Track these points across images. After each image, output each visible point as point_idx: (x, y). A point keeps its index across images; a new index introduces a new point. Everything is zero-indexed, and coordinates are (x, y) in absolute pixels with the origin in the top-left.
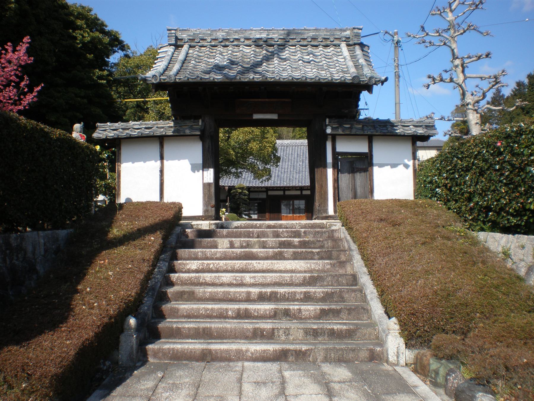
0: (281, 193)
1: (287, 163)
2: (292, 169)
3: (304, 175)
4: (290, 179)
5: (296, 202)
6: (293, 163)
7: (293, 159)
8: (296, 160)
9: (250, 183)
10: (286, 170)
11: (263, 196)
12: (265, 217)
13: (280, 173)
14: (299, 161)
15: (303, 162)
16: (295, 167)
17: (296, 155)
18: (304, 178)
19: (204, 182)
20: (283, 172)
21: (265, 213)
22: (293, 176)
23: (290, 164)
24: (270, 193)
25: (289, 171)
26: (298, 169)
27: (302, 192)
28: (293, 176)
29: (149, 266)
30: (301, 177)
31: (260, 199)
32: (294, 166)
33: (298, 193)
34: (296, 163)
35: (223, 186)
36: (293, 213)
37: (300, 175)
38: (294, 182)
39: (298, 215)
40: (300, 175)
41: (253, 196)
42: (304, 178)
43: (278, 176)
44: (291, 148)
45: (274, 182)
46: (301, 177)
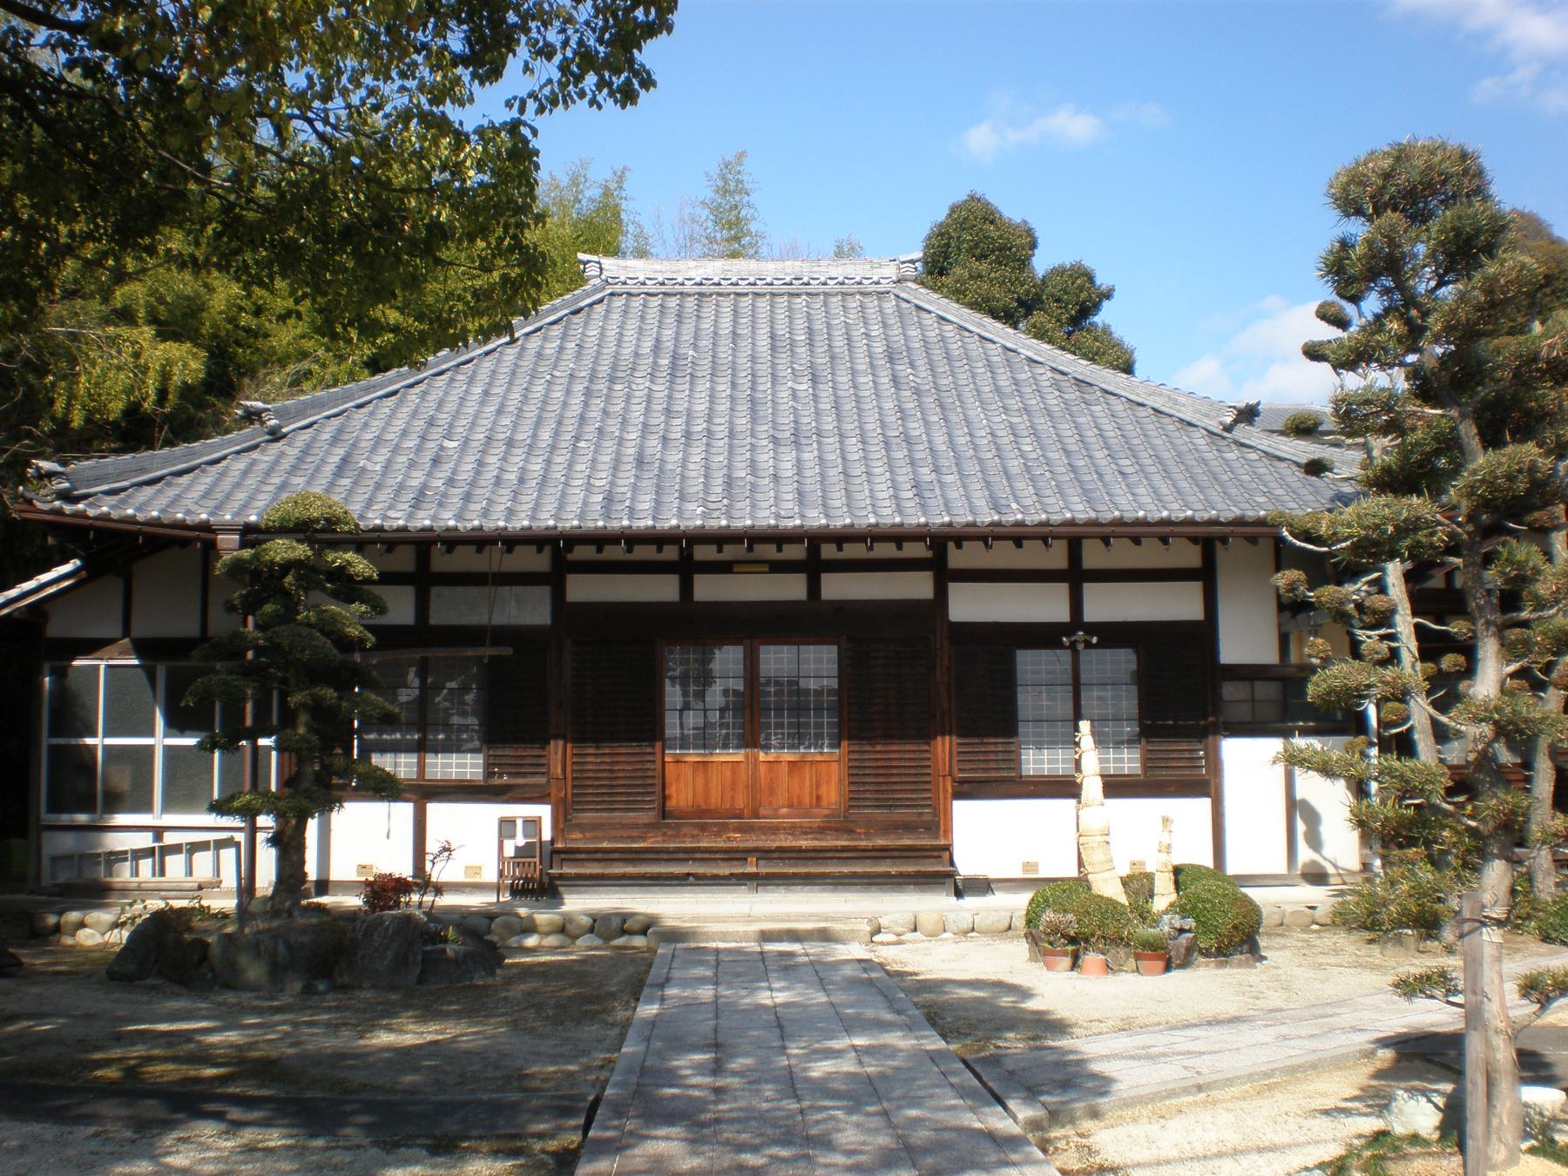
0: (664, 589)
1: (703, 386)
2: (742, 422)
3: (833, 456)
4: (729, 482)
5: (777, 660)
6: (744, 382)
7: (743, 361)
8: (764, 369)
9: (417, 503)
10: (699, 426)
11: (529, 610)
12: (540, 766)
13: (653, 443)
14: (784, 371)
15: (814, 380)
16: (766, 410)
17: (763, 343)
18: (834, 474)
19: (1205, 803)
20: (676, 433)
21: (544, 742)
22: (753, 466)
23: (724, 388)
24: (581, 589)
25: (721, 430)
26: (786, 419)
27: (814, 587)
28: (753, 466)
29: (57, 929)
30: (811, 471)
31: (502, 635)
32: (753, 401)
33: (792, 588)
34: (765, 385)
35: (205, 527)
36: (751, 739)
37: (809, 456)
38: (766, 498)
39: (788, 755)
40: (809, 456)
41: (450, 608)
42: (834, 474)
43: (640, 462)
44: (727, 305)
45: (609, 499)
46: (811, 471)
